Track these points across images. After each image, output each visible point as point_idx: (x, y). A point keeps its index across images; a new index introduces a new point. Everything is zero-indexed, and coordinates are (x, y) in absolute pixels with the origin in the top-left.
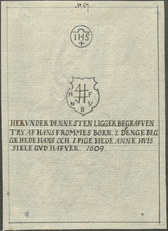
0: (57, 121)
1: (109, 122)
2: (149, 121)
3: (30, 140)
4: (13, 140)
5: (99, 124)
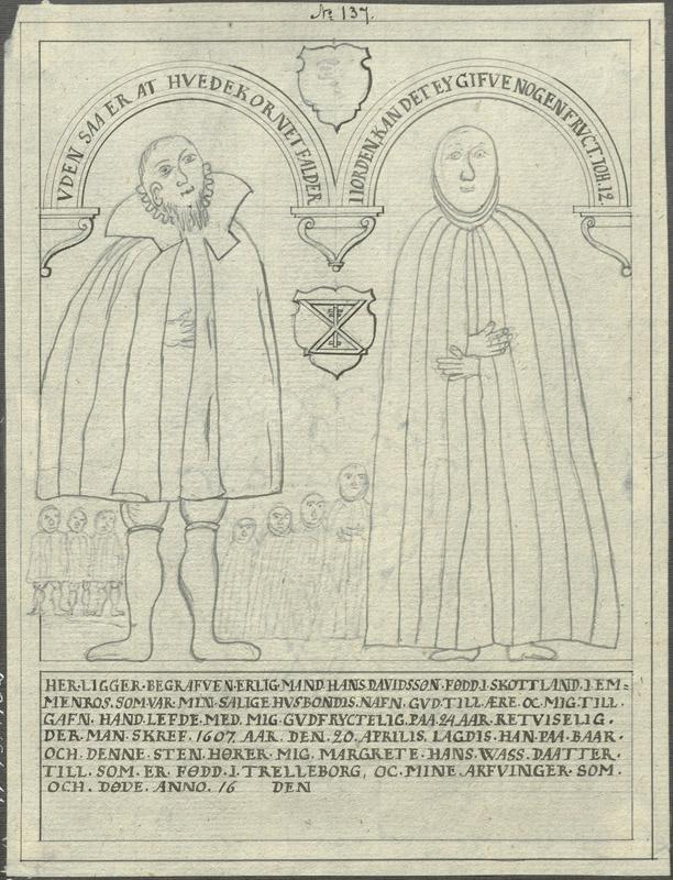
4: (542, 772)
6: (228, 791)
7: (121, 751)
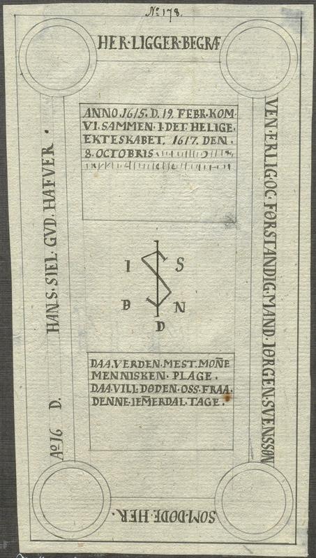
0: (169, 37)
1: (165, 40)
2: (208, 386)
3: (169, 126)
4: (210, 403)
5: (143, 45)
6: (179, 143)
7: (115, 399)
